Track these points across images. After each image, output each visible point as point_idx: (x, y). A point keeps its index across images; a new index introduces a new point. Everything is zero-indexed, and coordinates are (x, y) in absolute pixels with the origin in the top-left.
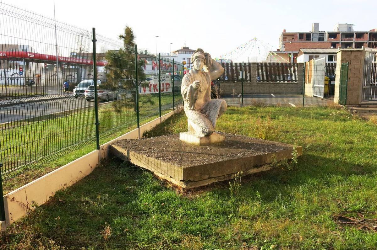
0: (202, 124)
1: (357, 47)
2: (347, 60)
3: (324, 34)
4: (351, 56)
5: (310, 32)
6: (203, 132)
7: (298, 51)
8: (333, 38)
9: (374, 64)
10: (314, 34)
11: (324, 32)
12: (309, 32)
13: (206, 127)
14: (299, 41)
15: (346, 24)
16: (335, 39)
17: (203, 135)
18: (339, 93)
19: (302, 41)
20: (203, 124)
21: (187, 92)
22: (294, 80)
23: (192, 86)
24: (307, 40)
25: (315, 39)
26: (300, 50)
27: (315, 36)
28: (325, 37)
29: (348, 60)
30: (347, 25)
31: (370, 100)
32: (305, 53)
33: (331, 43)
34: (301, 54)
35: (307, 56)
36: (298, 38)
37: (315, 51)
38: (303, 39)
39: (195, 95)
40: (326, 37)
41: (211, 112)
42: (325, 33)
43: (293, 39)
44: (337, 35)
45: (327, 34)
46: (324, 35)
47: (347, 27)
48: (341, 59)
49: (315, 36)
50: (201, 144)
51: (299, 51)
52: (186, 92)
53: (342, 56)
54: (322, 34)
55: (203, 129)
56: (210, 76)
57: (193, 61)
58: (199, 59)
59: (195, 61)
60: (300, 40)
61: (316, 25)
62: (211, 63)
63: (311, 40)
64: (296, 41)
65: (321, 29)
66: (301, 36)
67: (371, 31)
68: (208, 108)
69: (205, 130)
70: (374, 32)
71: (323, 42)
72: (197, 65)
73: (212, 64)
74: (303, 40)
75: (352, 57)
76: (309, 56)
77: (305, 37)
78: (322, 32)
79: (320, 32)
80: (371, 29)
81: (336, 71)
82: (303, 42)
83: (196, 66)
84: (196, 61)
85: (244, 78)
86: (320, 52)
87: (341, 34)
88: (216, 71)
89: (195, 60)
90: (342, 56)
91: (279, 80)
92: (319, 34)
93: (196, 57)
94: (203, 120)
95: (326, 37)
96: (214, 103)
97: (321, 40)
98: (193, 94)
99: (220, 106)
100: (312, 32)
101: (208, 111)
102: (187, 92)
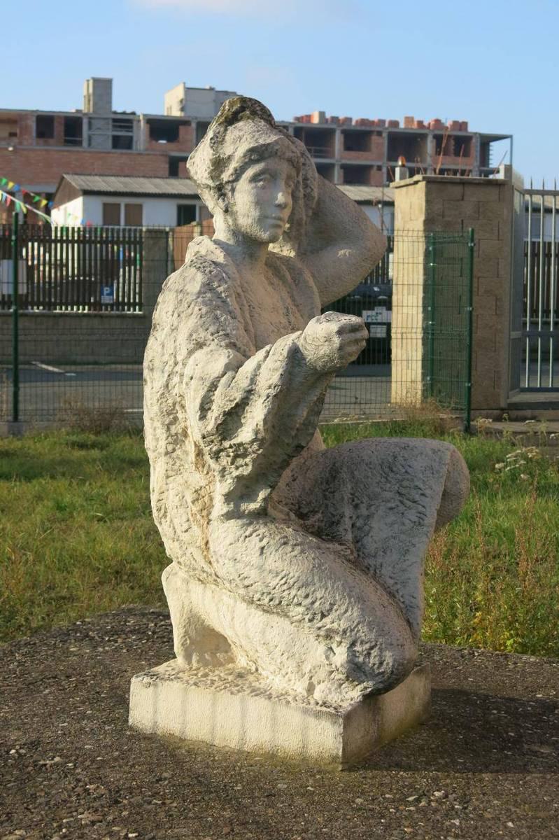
0: (344, 617)
1: (440, 173)
2: (447, 219)
3: (130, 121)
4: (462, 203)
5: (78, 111)
6: (355, 671)
7: (57, 185)
8: (164, 142)
9: (544, 243)
10: (93, 121)
11: (133, 114)
12: (74, 111)
13: (381, 633)
14: (38, 144)
15: (211, 89)
16: (172, 146)
17: (353, 694)
18: (424, 360)
19: (47, 144)
20: (355, 613)
21: (249, 392)
22: (123, 304)
23: (295, 355)
24: (67, 142)
25: (102, 138)
26: (63, 178)
27: (99, 129)
28: (134, 134)
29: (450, 219)
30: (212, 92)
31: (524, 390)
32: (86, 193)
33: (167, 160)
34: (71, 196)
35: (97, 203)
36: (34, 134)
37: (125, 184)
38: (51, 136)
39: (303, 413)
40: (141, 134)
41: (375, 524)
42: (136, 118)
43: (13, 135)
44: (182, 129)
45: (142, 123)
46: (131, 127)
47: (214, 101)
48: (422, 218)
49: (99, 129)
50: (354, 760)
51: (60, 185)
52: (238, 396)
53: (428, 201)
54: (125, 122)
55: (358, 648)
56: (311, 283)
57: (226, 176)
58: (272, 163)
59: (250, 172)
60: (41, 141)
61: (102, 88)
62: (315, 194)
63: (85, 144)
64: (25, 143)
65: (121, 103)
66: (46, 124)
67: (297, 119)
68: (347, 496)
69: (373, 660)
70: (309, 125)
71: (129, 151)
72: (259, 202)
73: (319, 203)
74: (51, 141)
75: (468, 208)
76: (105, 205)
77: (59, 129)
78: (124, 113)
79: (115, 113)
80: (299, 115)
81: (391, 266)
82: (56, 150)
83: (255, 213)
84: (254, 179)
85: (20, 292)
86: (96, 189)
87: (194, 125)
88: (343, 252)
89: (238, 174)
90: (428, 201)
91: (129, 304)
92: (115, 120)
93: (252, 150)
94: (349, 591)
95: (141, 134)
96: (389, 468)
97: (124, 143)
98: (297, 405)
99: (440, 490)
100: (86, 111)
101: (347, 519)
102: (249, 392)
